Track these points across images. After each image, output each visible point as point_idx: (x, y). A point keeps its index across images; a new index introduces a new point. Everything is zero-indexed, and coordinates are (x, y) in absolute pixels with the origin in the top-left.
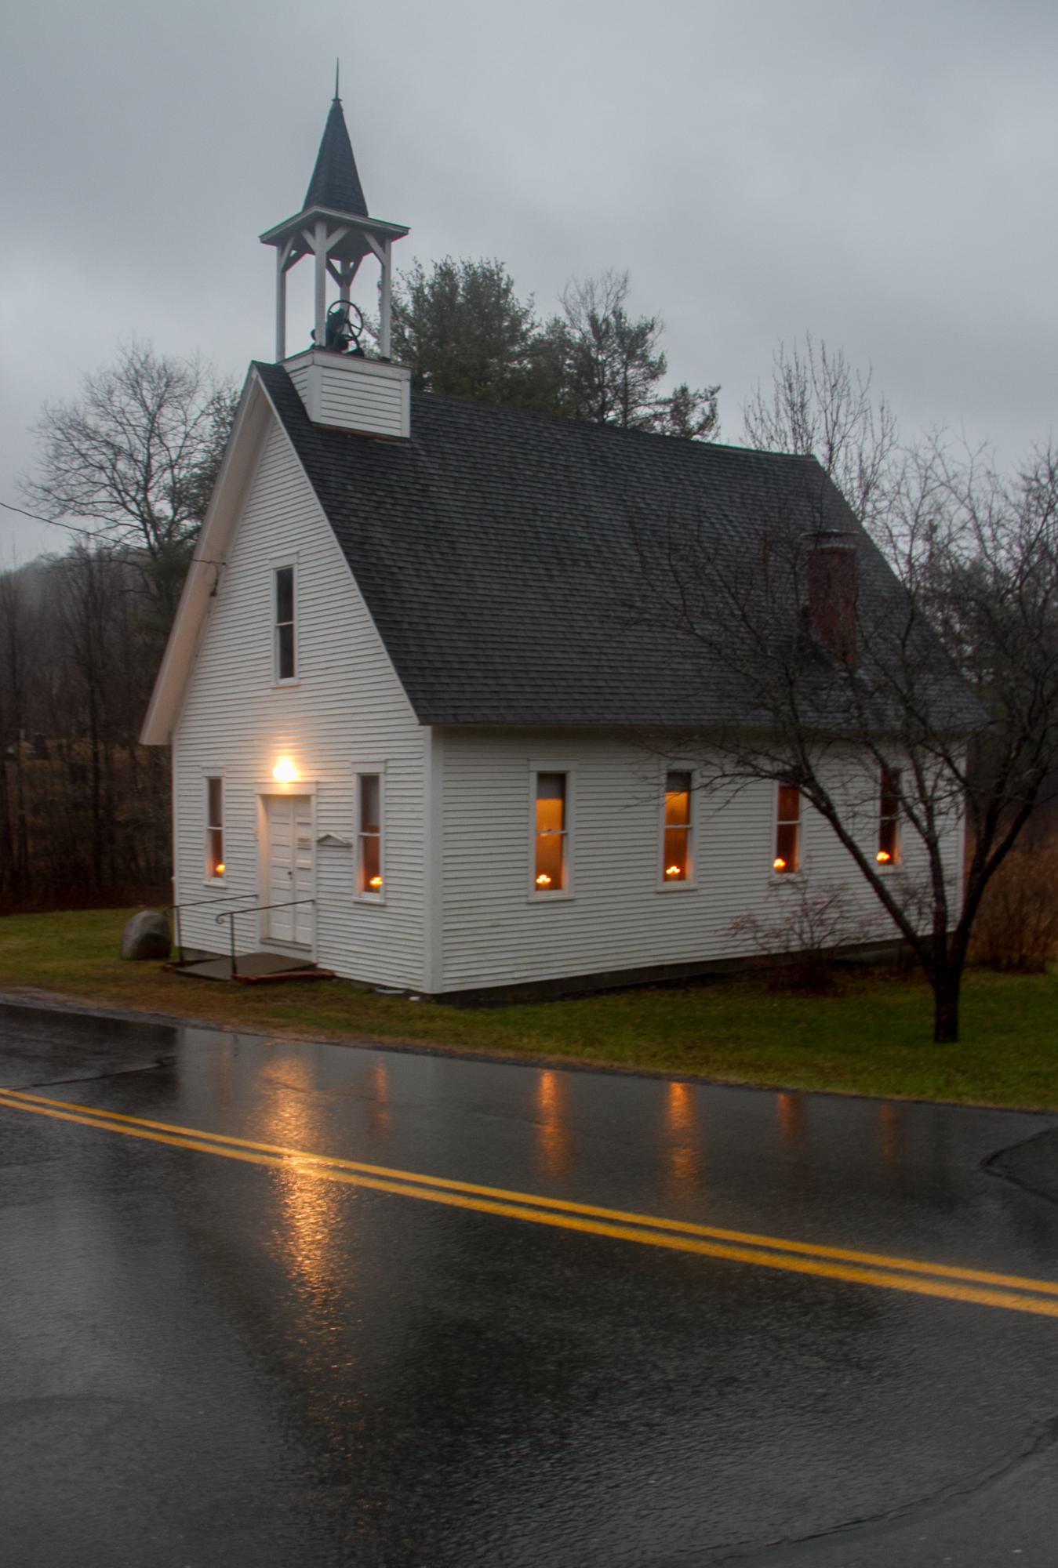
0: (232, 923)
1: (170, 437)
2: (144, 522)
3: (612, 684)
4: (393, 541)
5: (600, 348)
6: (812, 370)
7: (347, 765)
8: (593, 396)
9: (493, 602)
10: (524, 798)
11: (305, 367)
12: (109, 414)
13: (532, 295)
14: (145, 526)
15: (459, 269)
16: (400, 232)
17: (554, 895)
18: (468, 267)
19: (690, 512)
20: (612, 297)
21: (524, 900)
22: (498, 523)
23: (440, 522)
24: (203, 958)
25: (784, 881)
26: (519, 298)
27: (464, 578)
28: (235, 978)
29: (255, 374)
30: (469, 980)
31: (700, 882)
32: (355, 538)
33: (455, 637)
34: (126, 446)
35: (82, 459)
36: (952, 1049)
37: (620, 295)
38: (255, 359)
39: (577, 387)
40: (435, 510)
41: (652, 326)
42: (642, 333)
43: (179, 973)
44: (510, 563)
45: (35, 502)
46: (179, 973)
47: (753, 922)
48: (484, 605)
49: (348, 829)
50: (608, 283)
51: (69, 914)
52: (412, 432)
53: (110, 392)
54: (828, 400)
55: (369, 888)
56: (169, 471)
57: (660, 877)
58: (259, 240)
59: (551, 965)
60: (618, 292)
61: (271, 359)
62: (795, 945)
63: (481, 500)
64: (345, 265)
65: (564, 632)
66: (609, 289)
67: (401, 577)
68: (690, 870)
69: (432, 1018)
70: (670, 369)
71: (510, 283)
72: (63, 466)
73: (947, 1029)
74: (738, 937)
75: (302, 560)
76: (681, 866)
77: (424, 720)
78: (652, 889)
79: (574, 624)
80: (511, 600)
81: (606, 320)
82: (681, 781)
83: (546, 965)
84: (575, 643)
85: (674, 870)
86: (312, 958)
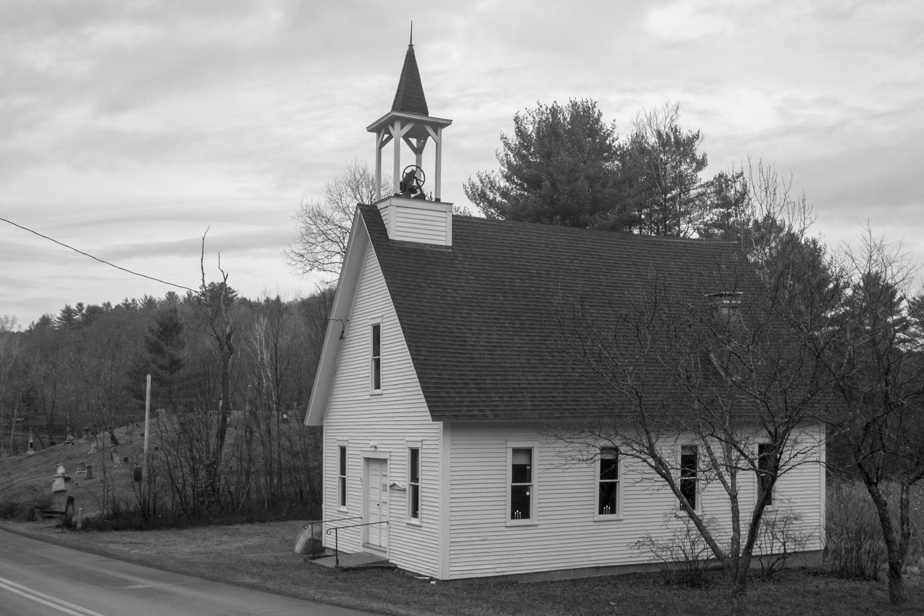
11: (387, 207)
13: (614, 121)
20: (668, 120)
26: (606, 121)
30: (466, 572)
42: (690, 142)
45: (295, 263)
46: (311, 563)
50: (666, 110)
58: (366, 130)
59: (521, 564)
64: (418, 142)
71: (600, 114)
72: (311, 240)
75: (385, 320)
77: (435, 418)
81: (668, 135)
83: (518, 565)
86: (386, 556)
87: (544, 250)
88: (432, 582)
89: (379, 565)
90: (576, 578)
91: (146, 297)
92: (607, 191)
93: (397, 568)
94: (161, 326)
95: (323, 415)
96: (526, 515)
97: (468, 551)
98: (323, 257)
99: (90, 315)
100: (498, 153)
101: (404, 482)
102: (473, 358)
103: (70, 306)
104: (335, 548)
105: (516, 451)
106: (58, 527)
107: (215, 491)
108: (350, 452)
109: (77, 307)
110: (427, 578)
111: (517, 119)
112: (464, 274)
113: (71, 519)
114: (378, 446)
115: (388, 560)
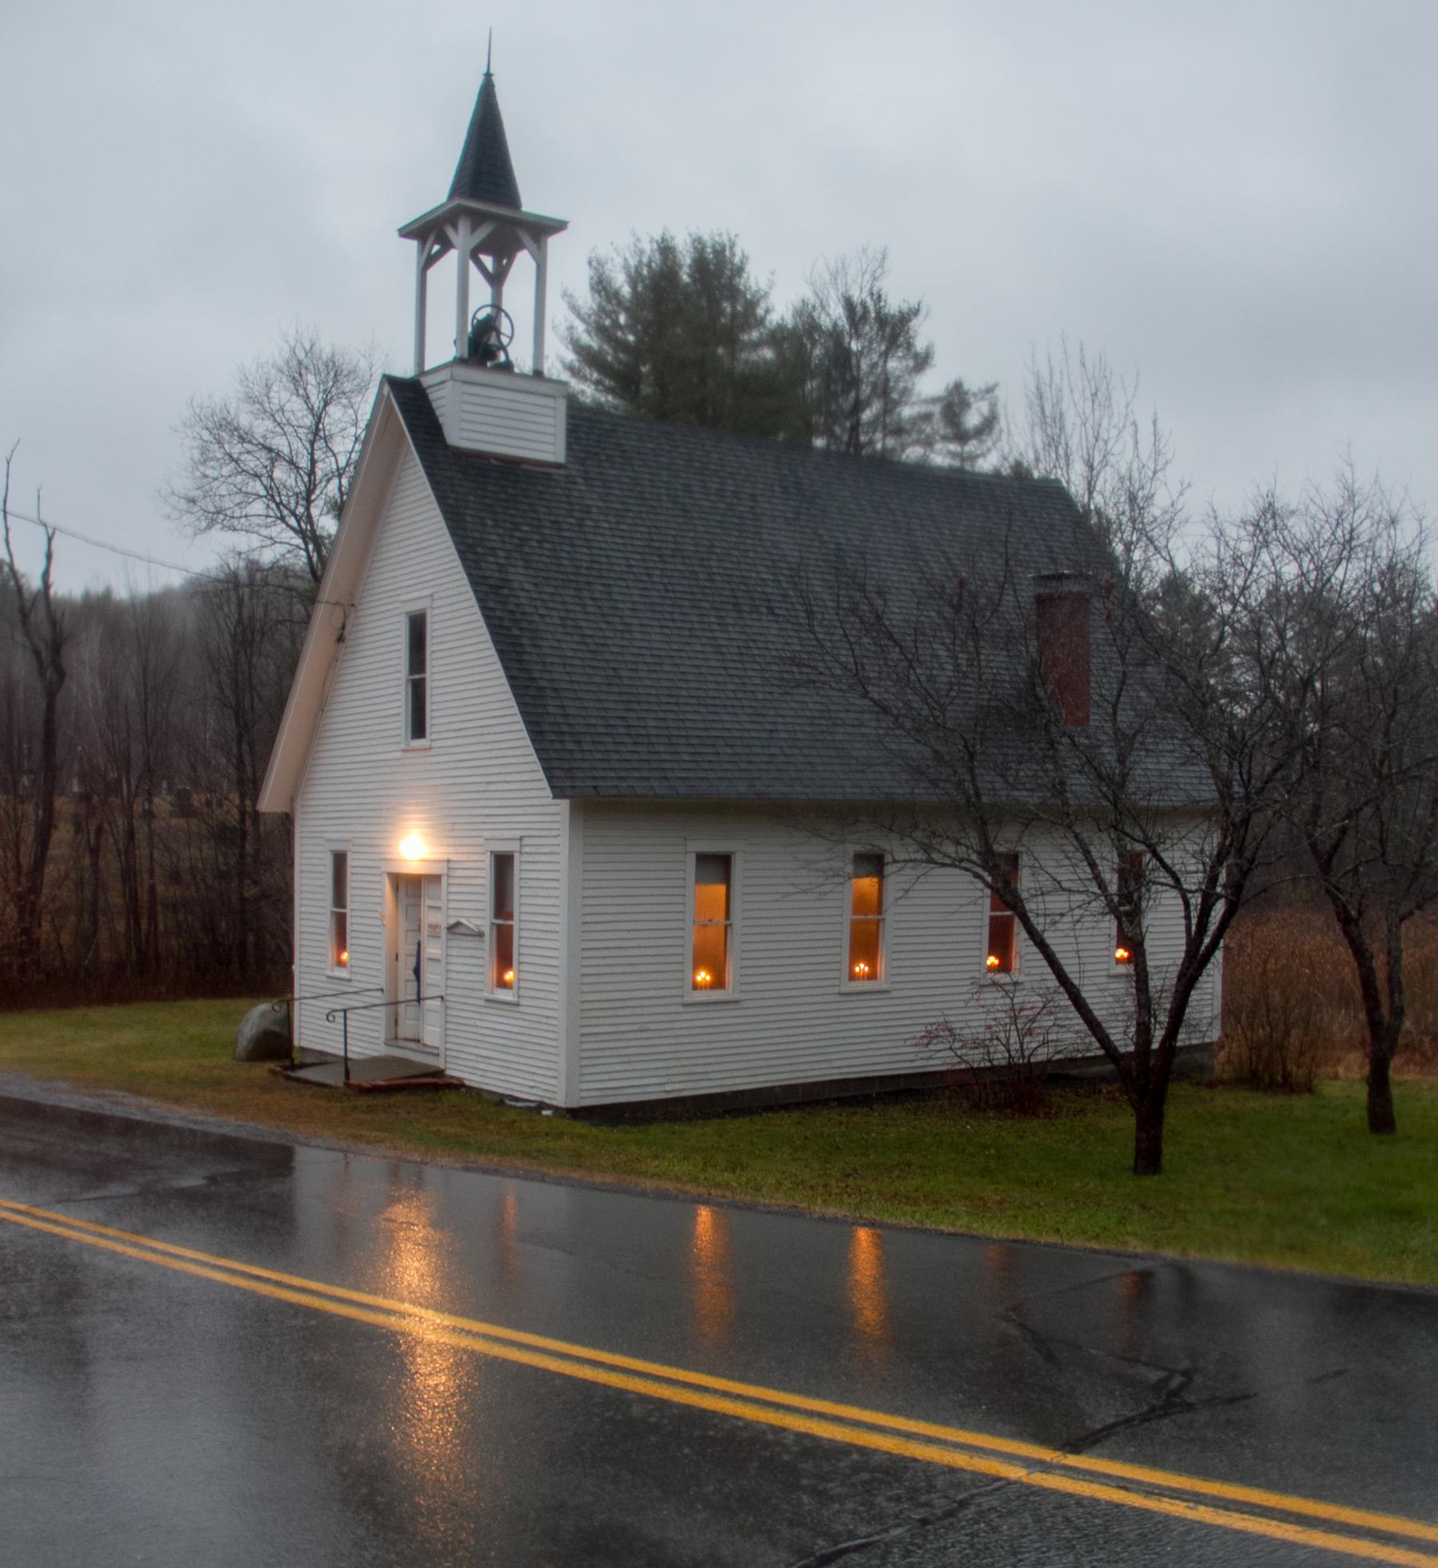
0: (345, 1018)
1: (338, 439)
2: (304, 538)
3: (788, 751)
4: (536, 585)
5: (857, 334)
6: (1069, 376)
7: (481, 841)
8: (846, 391)
9: (652, 656)
10: (681, 883)
12: (265, 411)
13: (772, 273)
14: (306, 544)
15: (706, 238)
16: (558, 226)
17: (1002, 978)
18: (699, 245)
19: (901, 548)
20: (867, 277)
22: (666, 562)
23: (596, 562)
24: (322, 1059)
25: (989, 982)
26: (755, 278)
27: (619, 627)
28: (347, 1085)
29: (387, 389)
32: (492, 582)
33: (603, 696)
34: (286, 451)
35: (233, 464)
36: (1150, 1182)
37: (877, 274)
38: (387, 373)
39: (828, 380)
40: (590, 548)
43: (288, 1078)
44: (676, 610)
46: (288, 1078)
47: (950, 1030)
48: (640, 659)
49: (481, 916)
51: (201, 1005)
52: (568, 456)
53: (268, 387)
54: (1088, 410)
55: (502, 984)
57: (846, 971)
58: (397, 234)
60: (875, 271)
61: (405, 369)
62: (1000, 1057)
63: (646, 536)
65: (734, 691)
66: (865, 266)
67: (542, 627)
68: (881, 968)
69: (560, 1136)
70: (938, 358)
71: (744, 258)
72: (209, 472)
73: (1148, 1159)
74: (931, 1047)
75: (437, 603)
76: (872, 963)
77: (558, 792)
78: (836, 990)
79: (747, 680)
80: (675, 654)
81: (863, 304)
82: (874, 863)
84: (746, 703)
85: (862, 968)
86: (439, 1063)
88: (545, 1112)
93: (463, 1085)
97: (614, 1052)
98: (232, 505)
104: (342, 1053)
108: (354, 863)
110: (532, 1105)
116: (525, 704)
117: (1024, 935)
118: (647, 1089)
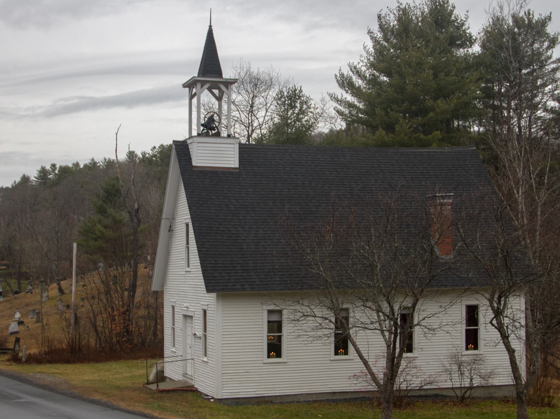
13: (467, 12)
21: (261, 362)
31: (419, 354)
38: (176, 139)
41: (550, 17)
42: (543, 23)
56: (261, 123)
78: (329, 359)
86: (193, 383)
87: (310, 166)
89: (185, 388)
90: (317, 399)
91: (105, 159)
92: (449, 79)
94: (106, 192)
95: (163, 284)
96: (279, 355)
99: (62, 175)
100: (365, 45)
101: (200, 333)
102: (243, 249)
103: (45, 167)
105: (270, 312)
106: (8, 360)
107: (128, 332)
109: (51, 168)
111: (379, 17)
112: (245, 187)
113: (18, 354)
114: (189, 307)
115: (193, 385)
116: (203, 260)
117: (351, 344)
118: (240, 393)
